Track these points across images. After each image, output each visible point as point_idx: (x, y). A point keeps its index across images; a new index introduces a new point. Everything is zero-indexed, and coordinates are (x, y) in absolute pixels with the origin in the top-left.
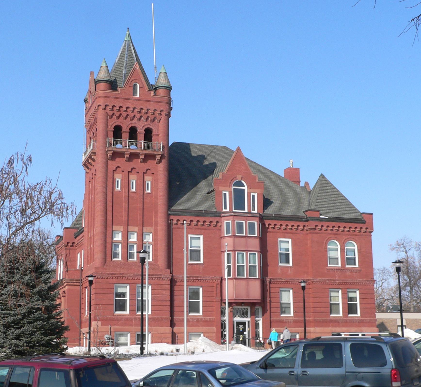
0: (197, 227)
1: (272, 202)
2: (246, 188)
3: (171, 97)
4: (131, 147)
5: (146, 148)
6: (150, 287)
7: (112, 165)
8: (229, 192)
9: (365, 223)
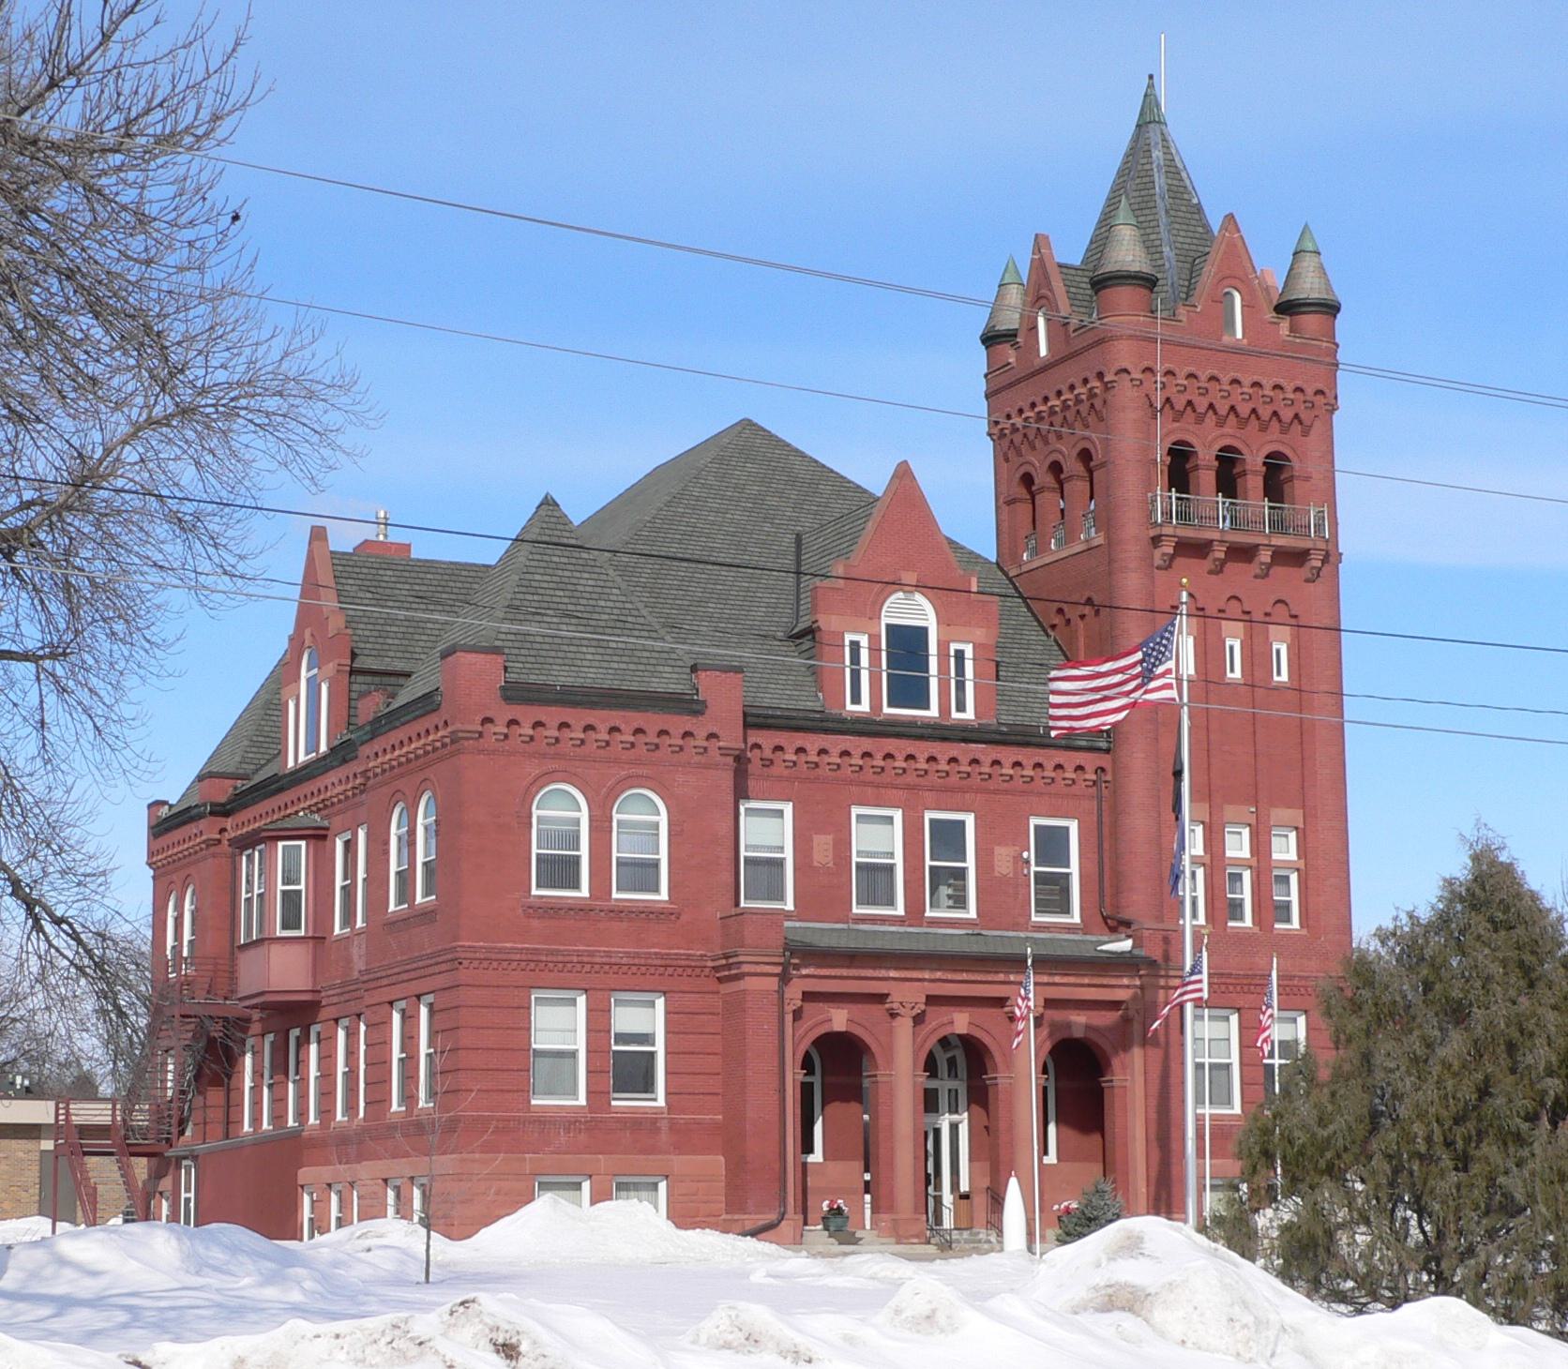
8: (870, 637)
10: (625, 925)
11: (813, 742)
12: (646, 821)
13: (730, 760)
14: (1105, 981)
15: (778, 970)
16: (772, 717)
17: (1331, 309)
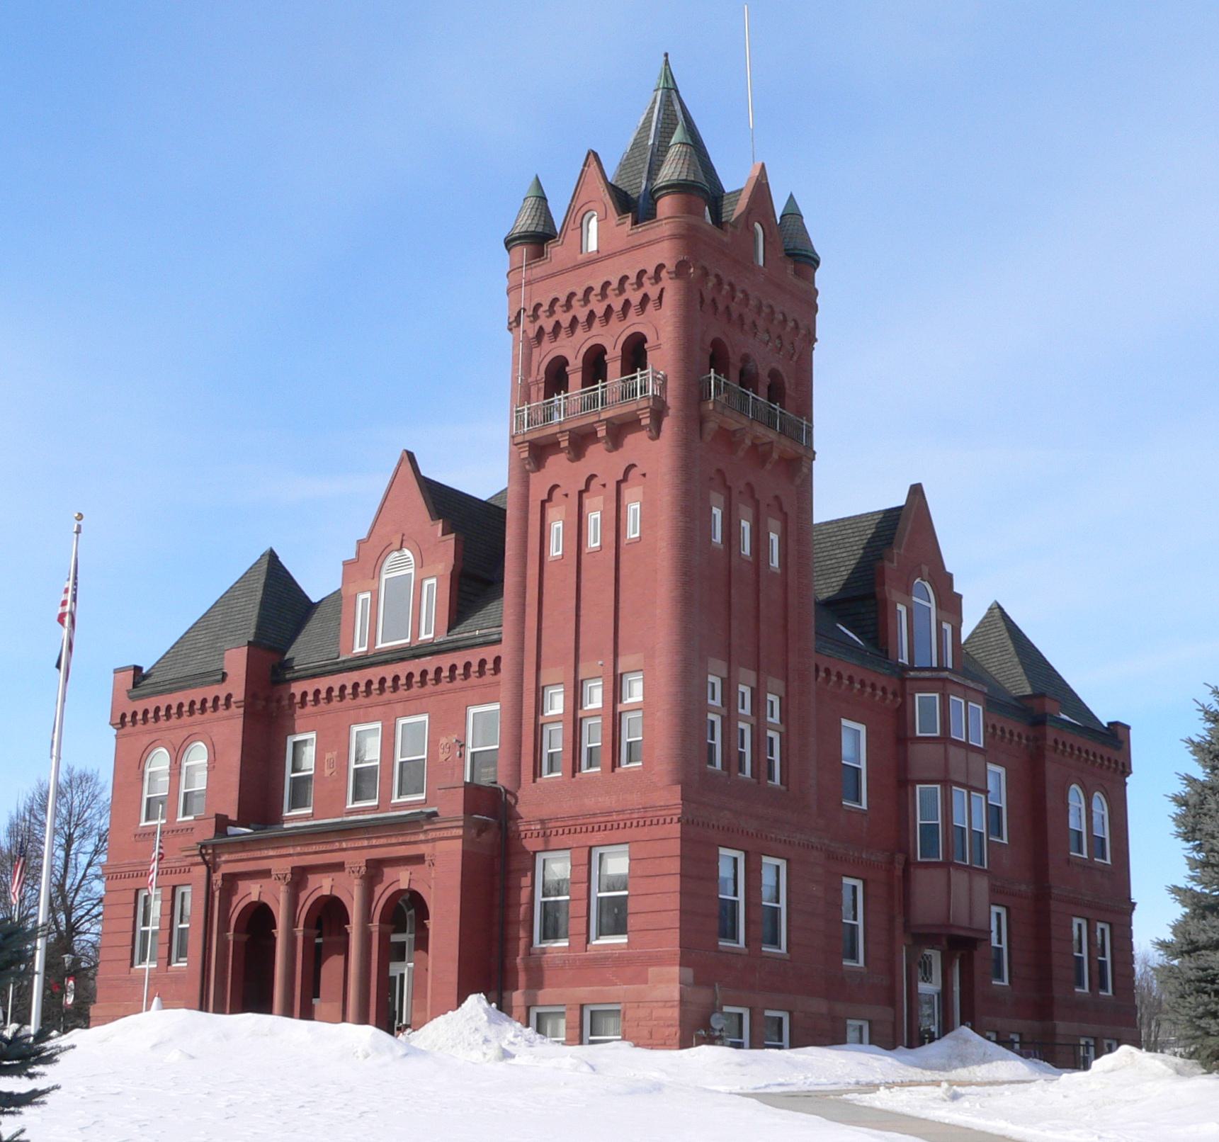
2: (933, 606)
14: (408, 839)
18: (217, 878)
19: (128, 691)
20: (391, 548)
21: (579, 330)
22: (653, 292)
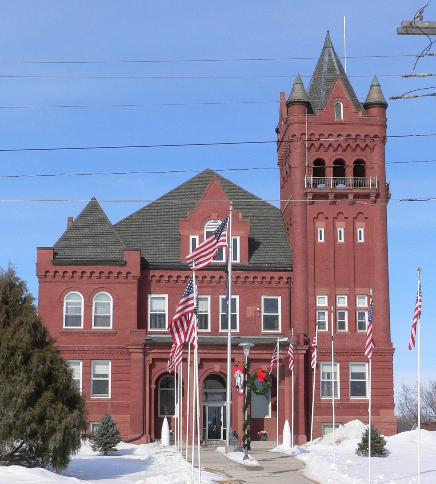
0: (63, 280)
1: (259, 243)
3: (387, 117)
4: (338, 187)
5: (357, 185)
6: (338, 365)
7: (312, 211)
9: (125, 265)
10: (96, 337)
11: (175, 274)
12: (105, 302)
13: (136, 281)
15: (142, 351)
16: (159, 265)
17: (384, 106)
18: (149, 359)
19: (52, 261)
20: (210, 218)
21: (331, 150)
22: (371, 145)
